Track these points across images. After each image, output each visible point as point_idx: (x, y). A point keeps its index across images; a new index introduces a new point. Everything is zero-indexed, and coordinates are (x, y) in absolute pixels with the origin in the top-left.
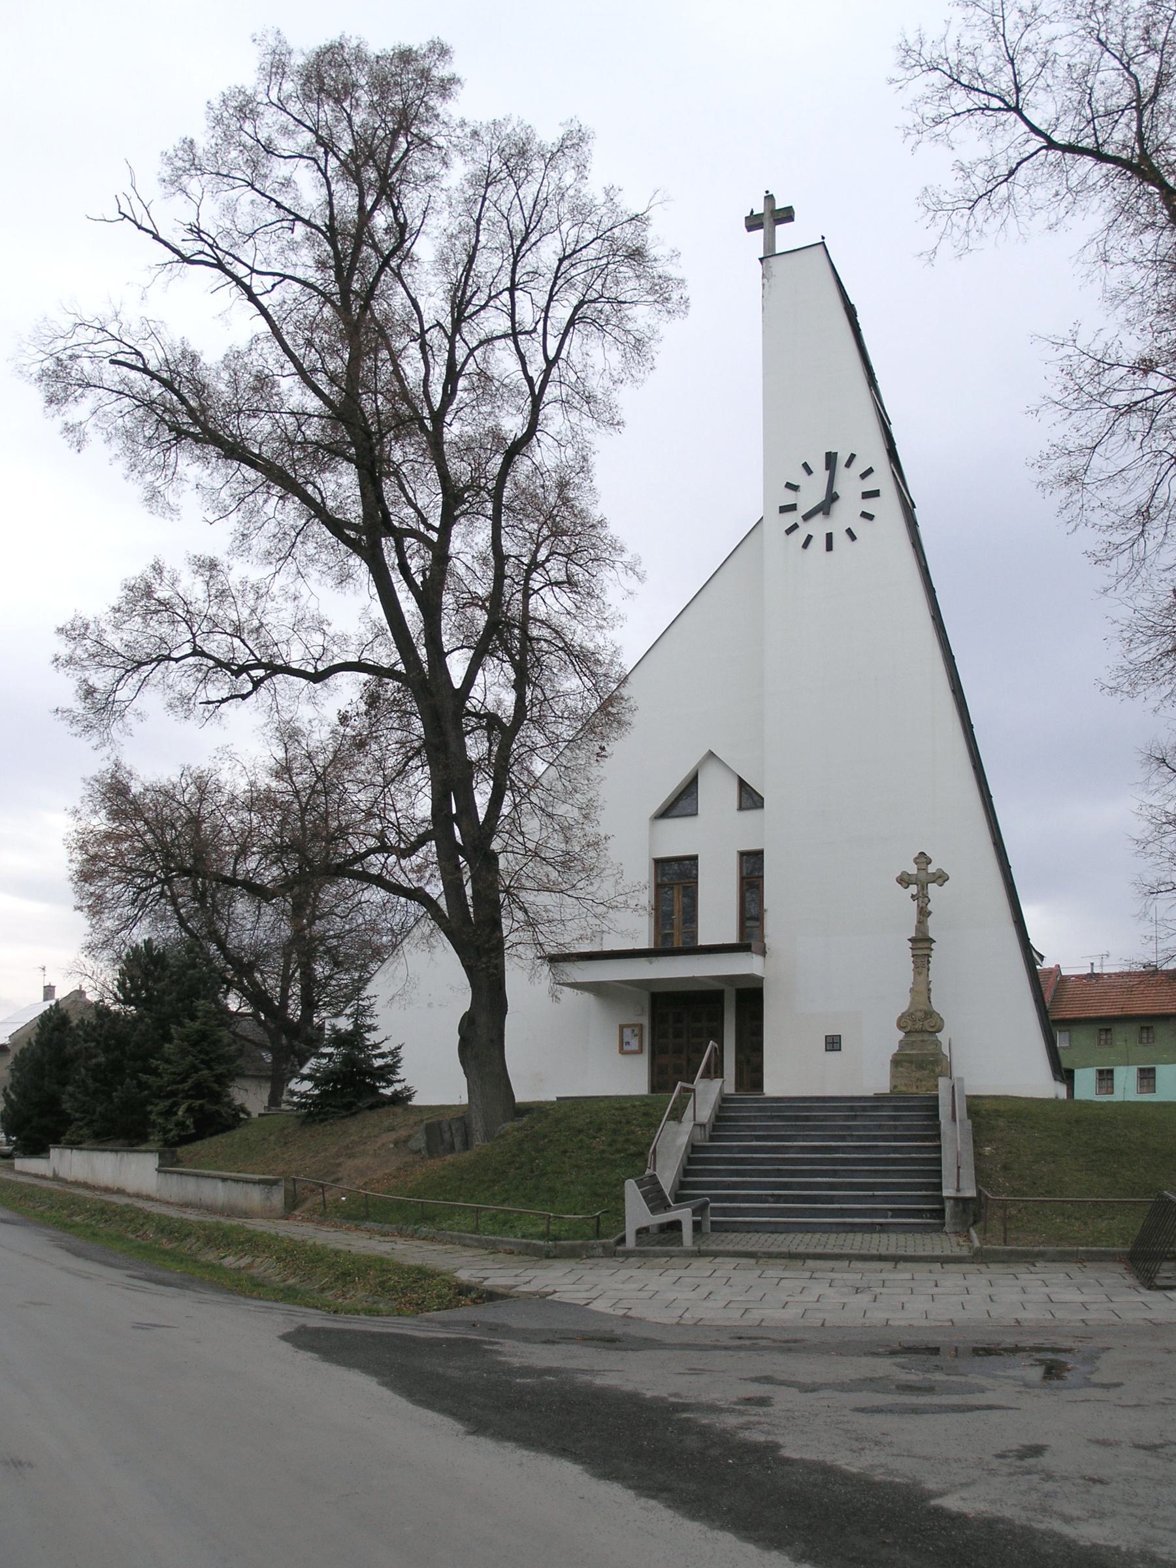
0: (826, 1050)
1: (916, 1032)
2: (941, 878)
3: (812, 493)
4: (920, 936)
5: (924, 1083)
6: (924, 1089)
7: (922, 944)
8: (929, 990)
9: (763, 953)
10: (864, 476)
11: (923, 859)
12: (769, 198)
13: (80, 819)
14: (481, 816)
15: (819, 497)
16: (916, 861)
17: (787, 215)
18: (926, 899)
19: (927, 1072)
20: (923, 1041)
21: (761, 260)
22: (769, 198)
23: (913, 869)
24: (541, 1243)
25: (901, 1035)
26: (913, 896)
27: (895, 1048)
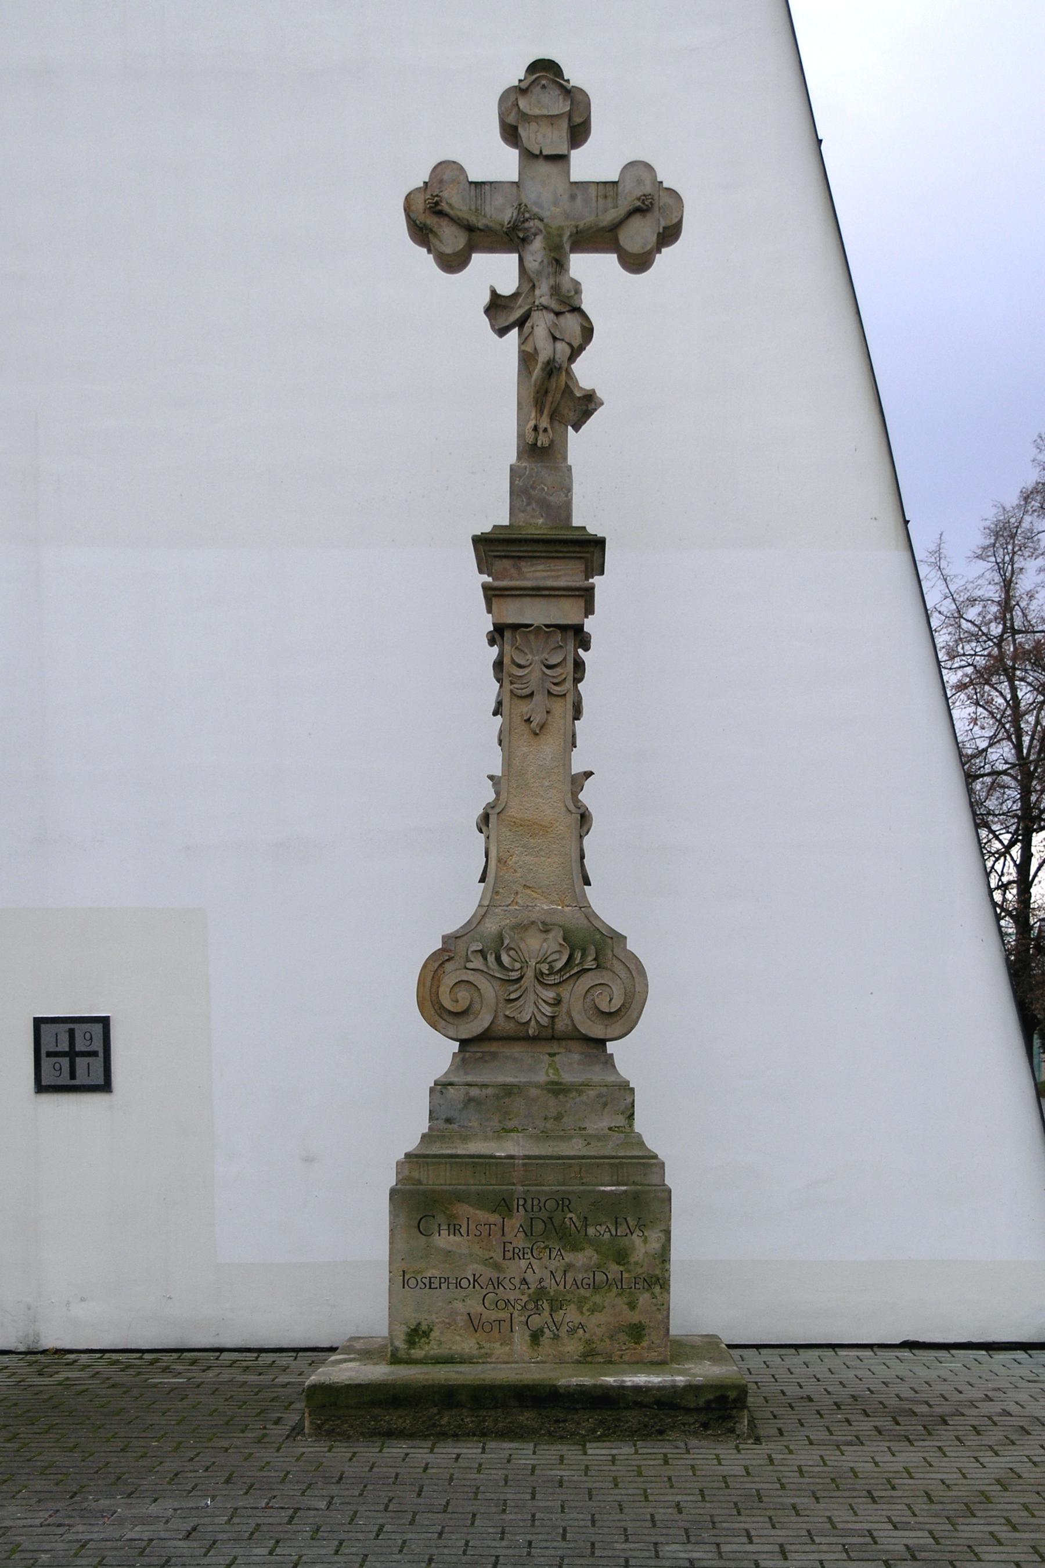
0: (41, 1088)
1: (521, 1037)
4: (538, 525)
5: (570, 1315)
6: (572, 1347)
13: (601, 488)
14: (1025, 755)
18: (571, 323)
19: (582, 1259)
20: (557, 1089)
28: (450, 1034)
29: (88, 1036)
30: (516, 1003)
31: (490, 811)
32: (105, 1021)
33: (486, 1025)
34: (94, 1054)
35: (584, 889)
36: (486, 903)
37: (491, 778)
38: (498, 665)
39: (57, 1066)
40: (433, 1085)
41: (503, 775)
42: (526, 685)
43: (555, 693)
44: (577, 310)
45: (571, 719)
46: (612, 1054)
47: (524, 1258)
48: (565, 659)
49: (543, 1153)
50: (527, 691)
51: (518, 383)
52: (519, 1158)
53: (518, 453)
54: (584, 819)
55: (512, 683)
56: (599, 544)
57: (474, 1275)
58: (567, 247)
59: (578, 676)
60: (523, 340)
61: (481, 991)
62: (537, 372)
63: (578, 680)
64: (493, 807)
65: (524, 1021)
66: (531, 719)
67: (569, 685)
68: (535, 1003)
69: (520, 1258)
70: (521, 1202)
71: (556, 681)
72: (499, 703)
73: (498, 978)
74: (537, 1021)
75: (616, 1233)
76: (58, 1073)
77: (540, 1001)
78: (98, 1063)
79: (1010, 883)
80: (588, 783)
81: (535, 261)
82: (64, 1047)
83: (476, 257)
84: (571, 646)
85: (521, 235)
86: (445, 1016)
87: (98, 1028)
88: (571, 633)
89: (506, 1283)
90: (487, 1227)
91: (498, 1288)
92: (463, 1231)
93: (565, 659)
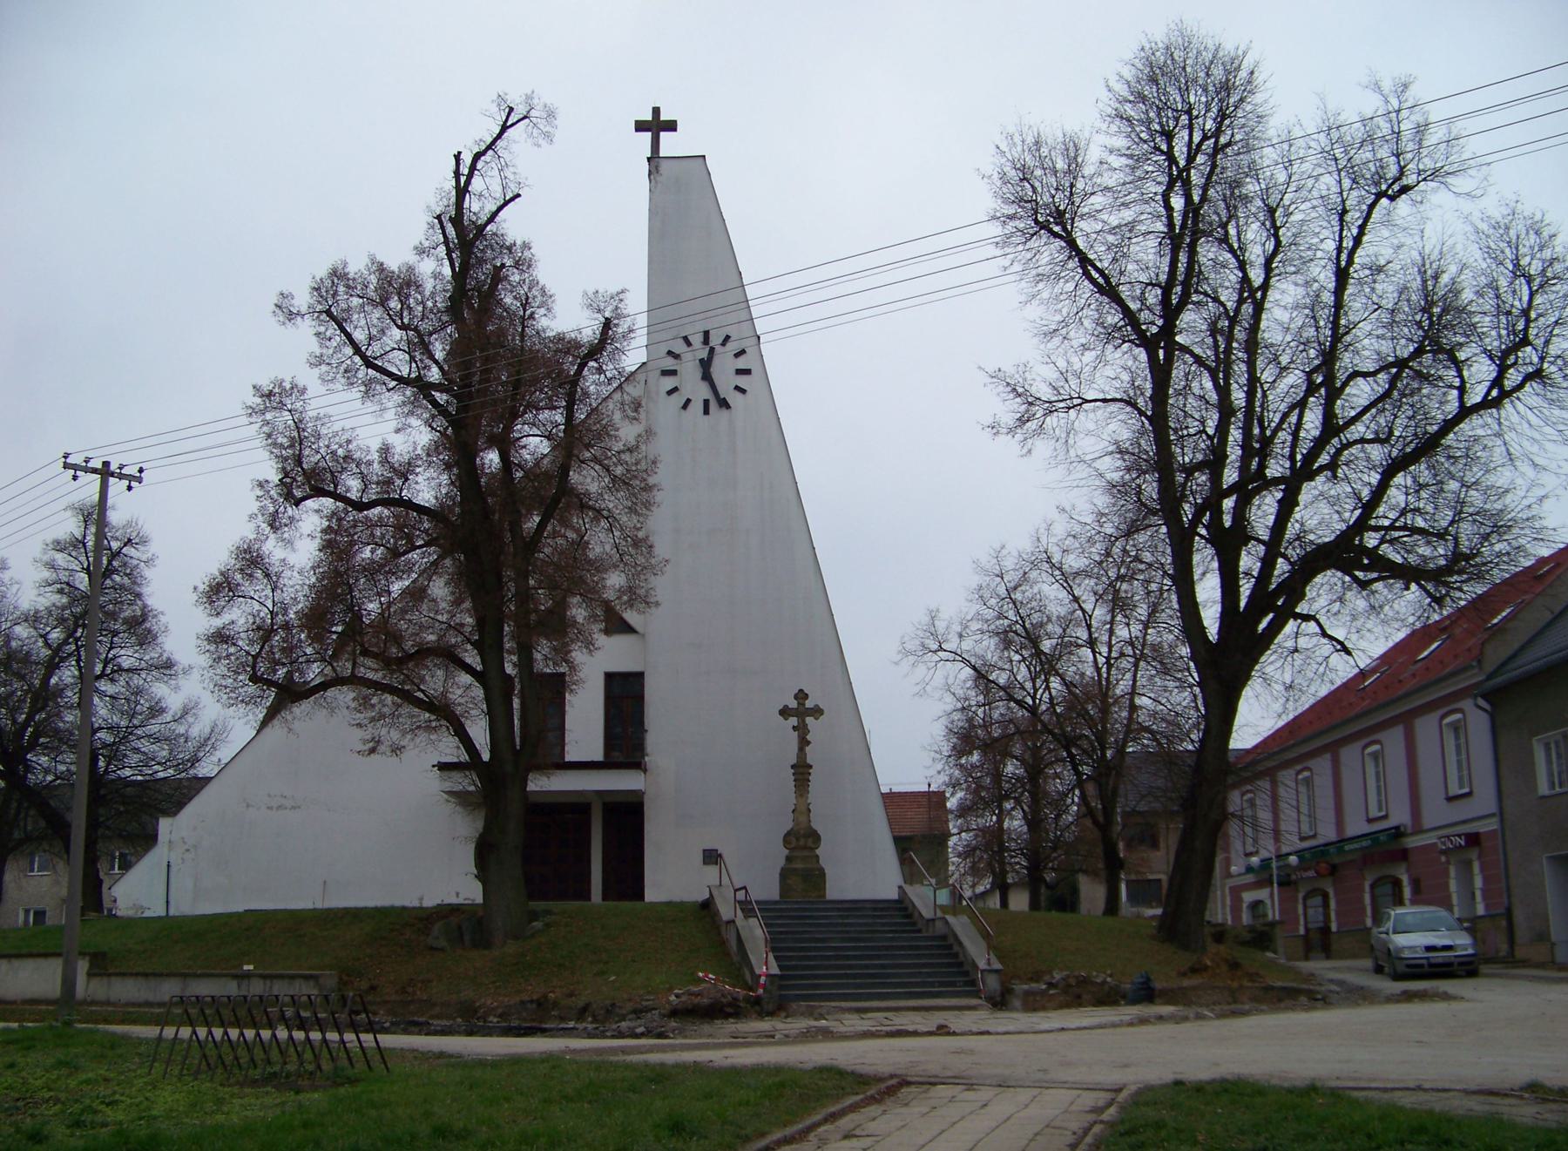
2: (817, 712)
3: (724, 369)
7: (802, 771)
8: (810, 811)
9: (645, 771)
10: (737, 355)
11: (801, 696)
12: (656, 111)
15: (716, 370)
16: (796, 697)
17: (671, 126)
21: (649, 159)
22: (656, 111)
23: (793, 704)
24: (1206, 1013)
25: (786, 852)
26: (794, 727)
27: (782, 862)
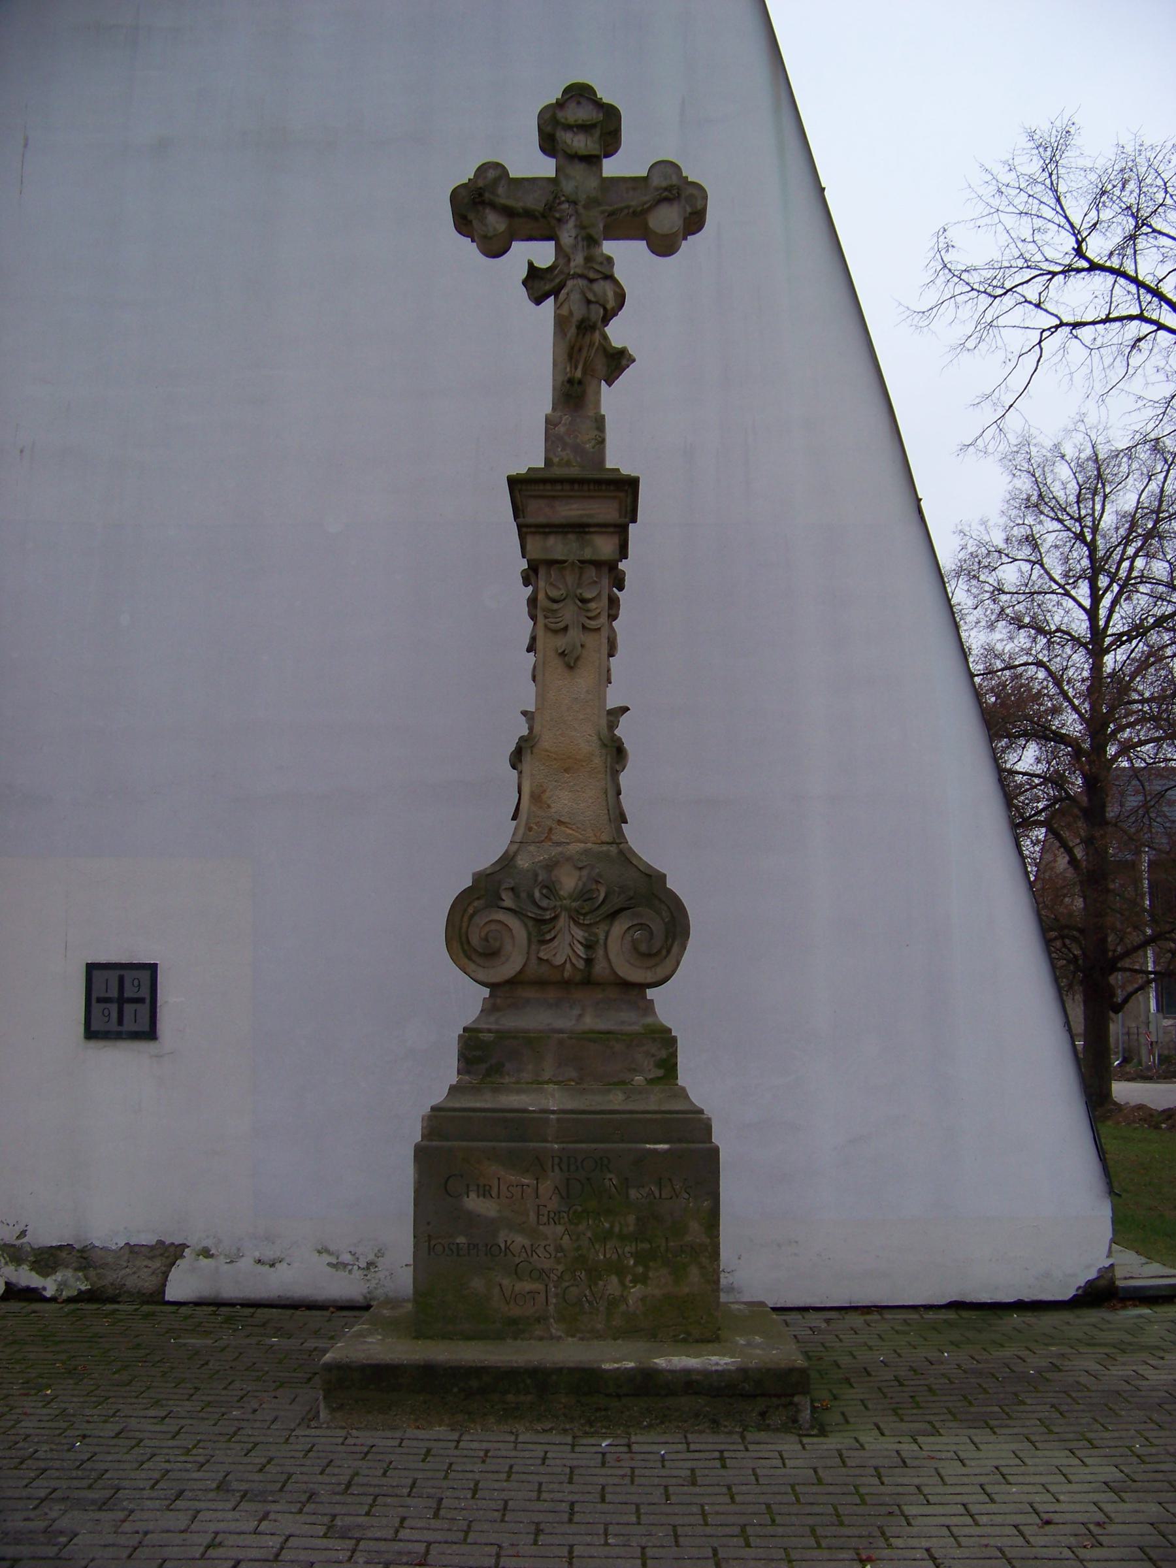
28: (481, 977)
29: (136, 983)
30: (550, 944)
31: (523, 745)
32: (153, 968)
33: (518, 968)
34: (141, 1000)
35: (621, 827)
36: (518, 839)
37: (524, 713)
38: (532, 602)
39: (106, 1013)
40: (462, 1032)
41: (537, 709)
42: (560, 619)
43: (588, 626)
44: (610, 278)
45: (606, 656)
46: (652, 1000)
47: (560, 1224)
48: (599, 594)
49: (582, 1107)
50: (562, 625)
51: (554, 333)
52: (553, 1112)
53: (553, 404)
54: (617, 753)
55: (546, 617)
56: (632, 484)
57: (506, 1241)
58: (708, 1145)
59: (613, 612)
60: (558, 307)
61: (514, 932)
62: (572, 331)
63: (614, 617)
64: (526, 740)
65: (558, 963)
66: (566, 652)
67: (603, 619)
68: (570, 945)
69: (555, 1223)
70: (556, 1160)
71: (590, 614)
72: (533, 639)
73: (531, 917)
74: (573, 965)
75: (660, 1194)
76: (106, 1019)
77: (575, 942)
78: (144, 1009)
79: (1132, 763)
80: (624, 719)
81: (570, 236)
82: (114, 993)
83: (516, 245)
84: (605, 582)
85: (557, 215)
86: (474, 957)
87: (145, 975)
88: (605, 570)
89: (540, 1251)
90: (519, 1188)
91: (532, 1255)
92: (494, 1193)
93: (599, 594)
